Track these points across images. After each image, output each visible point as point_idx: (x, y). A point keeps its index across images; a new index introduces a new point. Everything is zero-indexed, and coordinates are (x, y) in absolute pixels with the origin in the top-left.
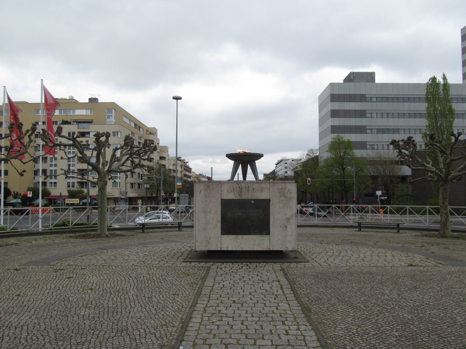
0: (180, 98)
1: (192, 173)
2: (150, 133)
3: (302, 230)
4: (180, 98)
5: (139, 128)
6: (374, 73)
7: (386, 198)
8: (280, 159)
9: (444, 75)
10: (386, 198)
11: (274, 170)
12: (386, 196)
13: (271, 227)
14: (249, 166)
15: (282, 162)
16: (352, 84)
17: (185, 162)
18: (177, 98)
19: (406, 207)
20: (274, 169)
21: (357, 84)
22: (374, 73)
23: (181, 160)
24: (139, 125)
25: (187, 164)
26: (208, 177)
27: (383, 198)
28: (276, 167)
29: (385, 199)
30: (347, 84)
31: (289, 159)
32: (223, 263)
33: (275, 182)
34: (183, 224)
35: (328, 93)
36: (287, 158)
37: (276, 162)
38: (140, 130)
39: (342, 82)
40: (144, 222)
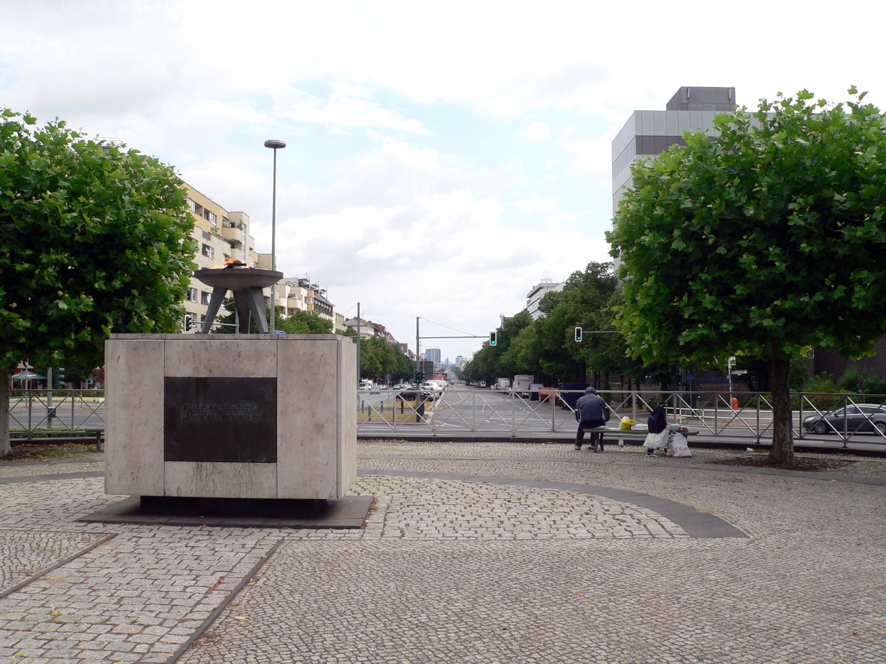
0: (282, 146)
1: (334, 315)
2: (233, 225)
3: (373, 448)
4: (282, 146)
5: (207, 213)
6: (733, 89)
7: (746, 372)
8: (536, 284)
9: (867, 93)
10: (746, 372)
11: (526, 309)
12: (745, 369)
13: (278, 439)
14: (686, 294)
15: (541, 290)
16: (684, 113)
17: (317, 291)
18: (274, 145)
19: (670, 394)
20: (526, 307)
21: (694, 113)
22: (733, 89)
23: (308, 286)
24: (205, 205)
25: (324, 295)
26: (375, 325)
27: (739, 373)
28: (528, 302)
29: (743, 375)
30: (673, 113)
31: (557, 284)
32: (299, 527)
33: (291, 336)
34: (572, 447)
35: (631, 135)
36: (554, 282)
37: (530, 289)
38: (208, 218)
39: (665, 109)
40: (27, 428)
